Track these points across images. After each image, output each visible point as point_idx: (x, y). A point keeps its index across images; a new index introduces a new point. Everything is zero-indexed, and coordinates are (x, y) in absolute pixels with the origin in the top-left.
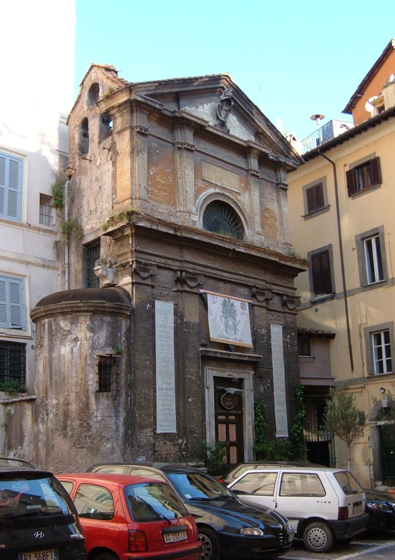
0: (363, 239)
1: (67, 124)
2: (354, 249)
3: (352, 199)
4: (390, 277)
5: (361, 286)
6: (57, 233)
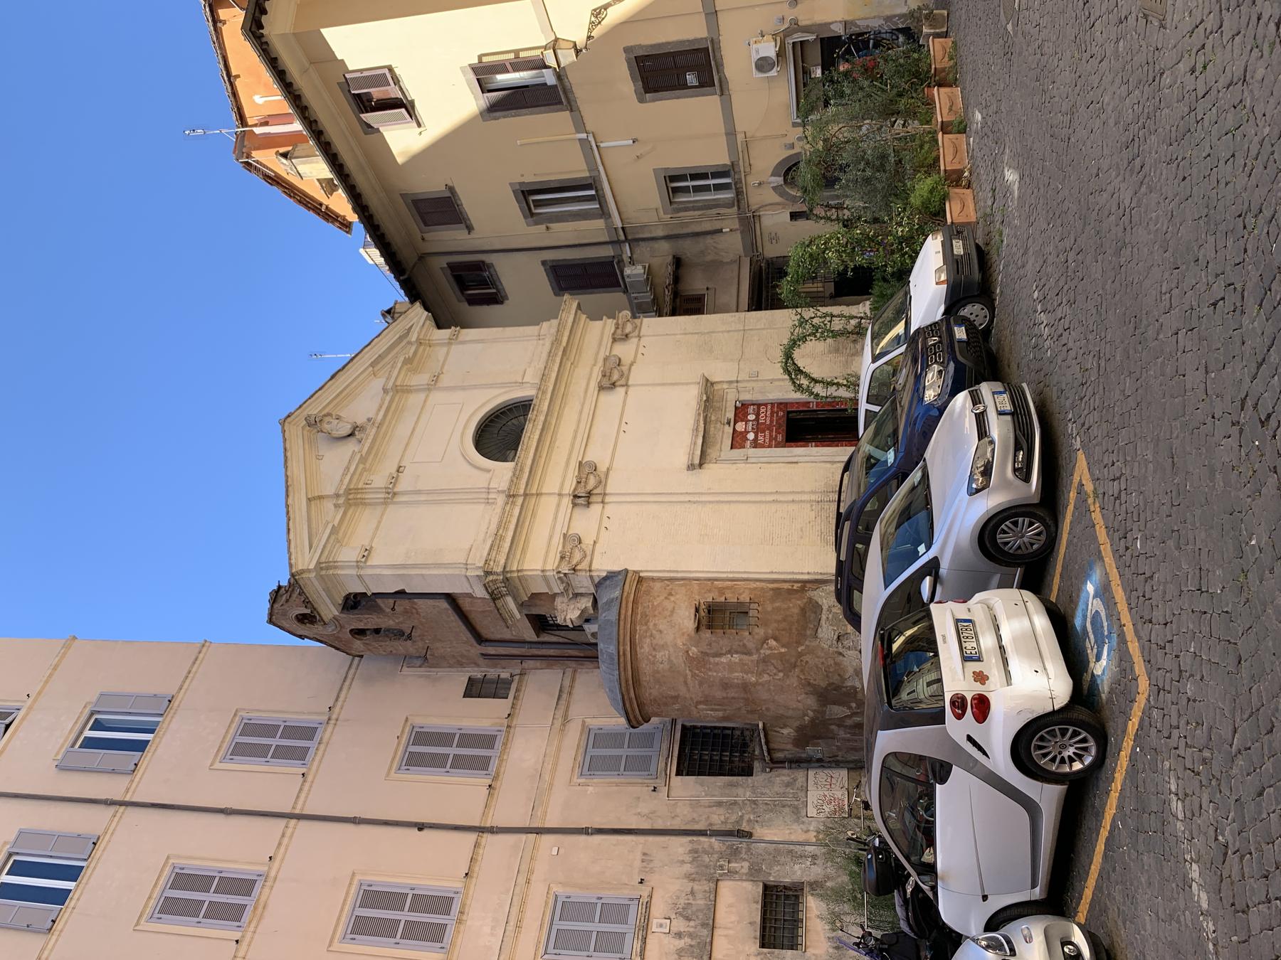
0: (532, 214)
1: (362, 656)
2: (547, 228)
3: (508, 299)
4: (587, 174)
5: (601, 218)
6: (703, 852)
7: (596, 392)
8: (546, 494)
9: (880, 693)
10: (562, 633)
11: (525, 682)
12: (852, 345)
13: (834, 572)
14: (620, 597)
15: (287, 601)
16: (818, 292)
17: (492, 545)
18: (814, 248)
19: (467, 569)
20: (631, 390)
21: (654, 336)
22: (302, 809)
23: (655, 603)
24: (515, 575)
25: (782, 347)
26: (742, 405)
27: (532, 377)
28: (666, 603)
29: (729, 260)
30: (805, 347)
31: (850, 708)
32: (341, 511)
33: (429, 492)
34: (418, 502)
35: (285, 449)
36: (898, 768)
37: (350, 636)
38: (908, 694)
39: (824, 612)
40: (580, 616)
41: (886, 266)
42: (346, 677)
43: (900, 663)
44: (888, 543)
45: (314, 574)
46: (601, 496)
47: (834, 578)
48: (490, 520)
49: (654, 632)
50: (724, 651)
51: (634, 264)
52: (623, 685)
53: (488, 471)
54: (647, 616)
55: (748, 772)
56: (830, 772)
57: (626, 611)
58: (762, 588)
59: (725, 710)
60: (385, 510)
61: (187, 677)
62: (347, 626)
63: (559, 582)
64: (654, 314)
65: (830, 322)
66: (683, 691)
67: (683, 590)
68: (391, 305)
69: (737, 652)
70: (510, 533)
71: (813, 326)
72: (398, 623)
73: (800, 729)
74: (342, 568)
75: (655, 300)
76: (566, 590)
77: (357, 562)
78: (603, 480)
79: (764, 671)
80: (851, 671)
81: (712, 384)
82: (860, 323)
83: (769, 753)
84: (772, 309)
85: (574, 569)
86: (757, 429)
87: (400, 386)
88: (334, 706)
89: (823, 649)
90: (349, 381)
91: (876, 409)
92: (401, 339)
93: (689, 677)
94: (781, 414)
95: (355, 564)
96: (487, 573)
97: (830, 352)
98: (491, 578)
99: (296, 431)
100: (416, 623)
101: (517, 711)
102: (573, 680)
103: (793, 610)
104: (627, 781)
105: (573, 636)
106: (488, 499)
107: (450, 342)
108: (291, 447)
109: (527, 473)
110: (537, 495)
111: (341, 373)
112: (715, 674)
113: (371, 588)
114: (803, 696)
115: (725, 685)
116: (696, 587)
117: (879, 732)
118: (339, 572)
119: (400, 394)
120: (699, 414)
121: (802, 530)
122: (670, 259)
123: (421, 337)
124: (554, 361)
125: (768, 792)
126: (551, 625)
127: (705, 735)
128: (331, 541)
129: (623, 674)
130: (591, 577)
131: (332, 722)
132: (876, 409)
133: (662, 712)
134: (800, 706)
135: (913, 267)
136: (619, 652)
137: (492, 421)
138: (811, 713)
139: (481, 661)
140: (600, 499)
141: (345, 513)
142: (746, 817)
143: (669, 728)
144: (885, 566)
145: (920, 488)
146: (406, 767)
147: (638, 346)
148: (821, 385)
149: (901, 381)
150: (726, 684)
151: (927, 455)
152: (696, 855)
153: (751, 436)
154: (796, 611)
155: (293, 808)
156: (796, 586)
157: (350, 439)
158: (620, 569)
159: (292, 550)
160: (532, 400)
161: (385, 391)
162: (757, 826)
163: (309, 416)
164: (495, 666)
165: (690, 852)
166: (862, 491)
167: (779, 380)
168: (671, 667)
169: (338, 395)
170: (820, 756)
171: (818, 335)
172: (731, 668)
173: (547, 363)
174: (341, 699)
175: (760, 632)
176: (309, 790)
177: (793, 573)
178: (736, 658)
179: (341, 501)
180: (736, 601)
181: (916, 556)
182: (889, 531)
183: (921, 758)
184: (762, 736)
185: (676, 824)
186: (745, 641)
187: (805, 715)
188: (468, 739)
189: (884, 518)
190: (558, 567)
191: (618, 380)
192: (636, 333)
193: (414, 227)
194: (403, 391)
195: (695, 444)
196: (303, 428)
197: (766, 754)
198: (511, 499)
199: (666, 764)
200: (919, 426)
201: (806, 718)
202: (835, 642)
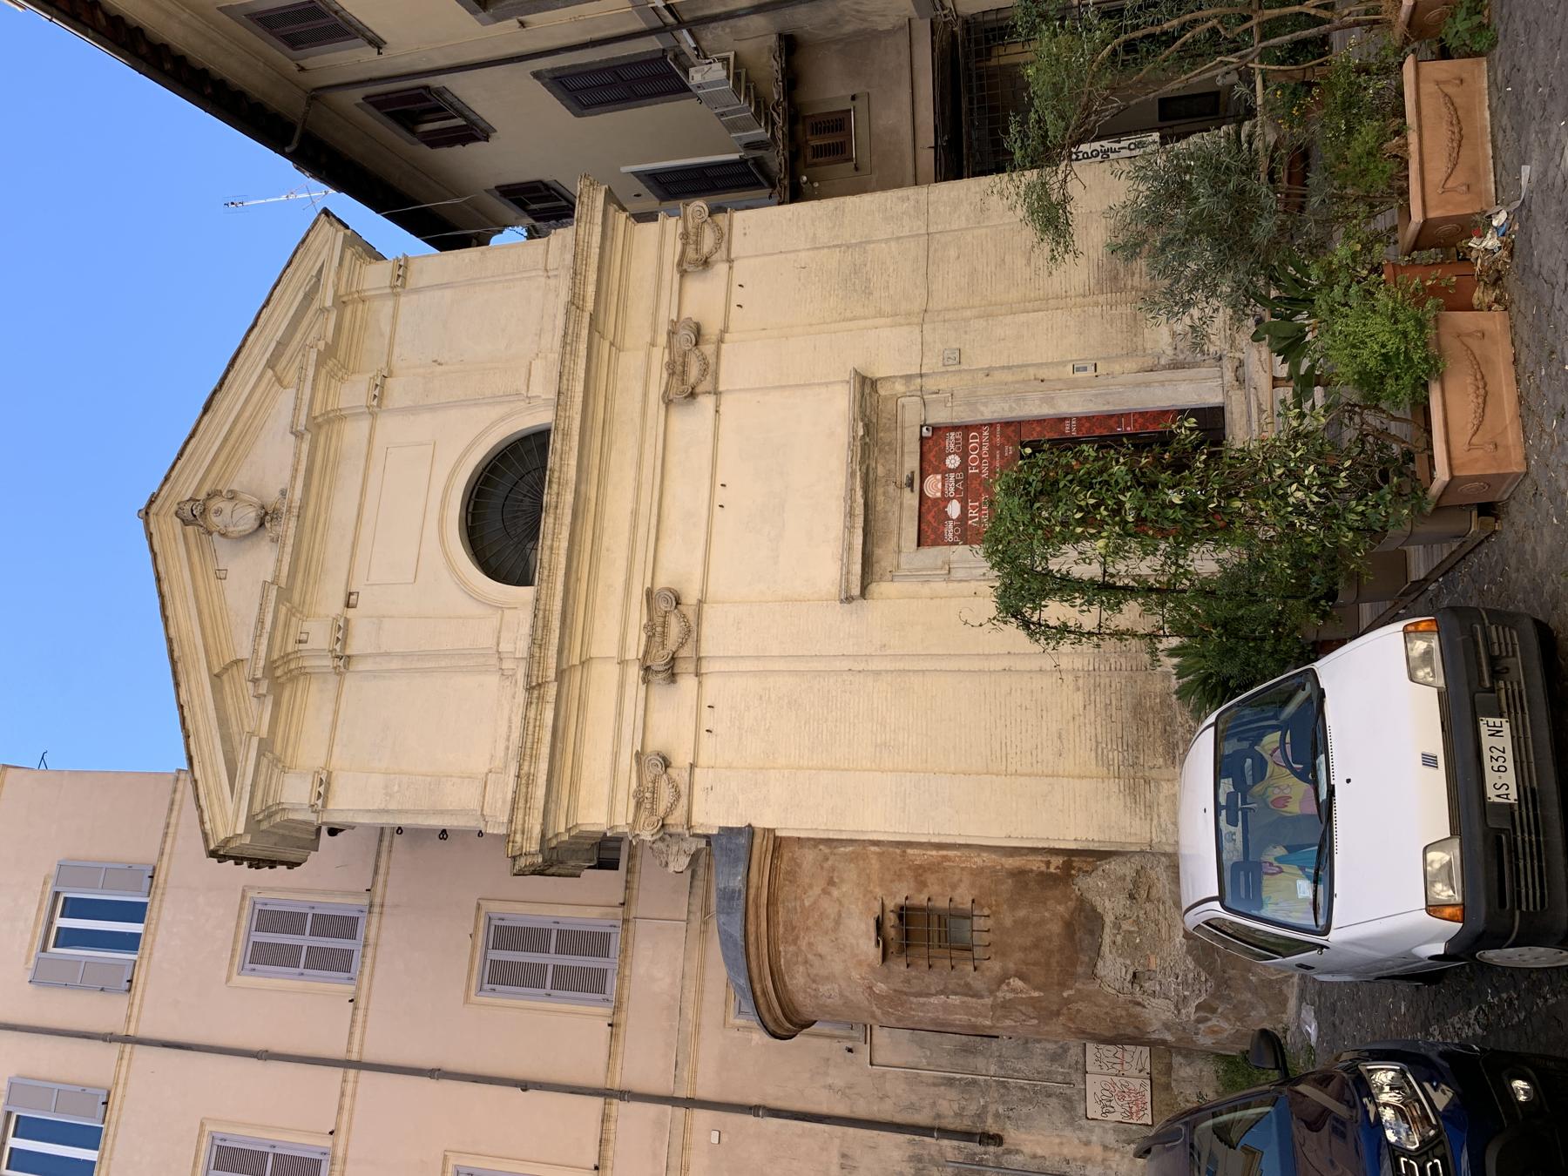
2: (522, 24)
6: (930, 1161)
20: (727, 402)
22: (360, 1053)
23: (807, 904)
27: (542, 387)
29: (889, 27)
32: (269, 701)
39: (1107, 930)
49: (810, 956)
50: (933, 991)
54: (794, 928)
57: (758, 926)
61: (166, 834)
69: (956, 994)
70: (543, 766)
81: (874, 383)
86: (966, 490)
87: (322, 415)
88: (373, 884)
89: (1106, 996)
90: (238, 407)
99: (168, 527)
101: (635, 892)
108: (167, 572)
109: (558, 631)
111: (219, 396)
116: (875, 864)
119: (325, 428)
120: (853, 474)
121: (1060, 737)
122: (773, 40)
124: (574, 353)
125: (1023, 1067)
128: (263, 769)
131: (376, 909)
141: (277, 704)
142: (992, 1108)
152: (920, 1166)
153: (954, 509)
154: (1056, 928)
155: (349, 1051)
159: (203, 802)
162: (1008, 1125)
165: (911, 1159)
169: (226, 439)
173: (562, 362)
174: (382, 871)
175: (995, 966)
176: (365, 1022)
185: (885, 1111)
188: (574, 941)
191: (699, 381)
192: (722, 253)
193: (278, 54)
194: (329, 421)
195: (850, 548)
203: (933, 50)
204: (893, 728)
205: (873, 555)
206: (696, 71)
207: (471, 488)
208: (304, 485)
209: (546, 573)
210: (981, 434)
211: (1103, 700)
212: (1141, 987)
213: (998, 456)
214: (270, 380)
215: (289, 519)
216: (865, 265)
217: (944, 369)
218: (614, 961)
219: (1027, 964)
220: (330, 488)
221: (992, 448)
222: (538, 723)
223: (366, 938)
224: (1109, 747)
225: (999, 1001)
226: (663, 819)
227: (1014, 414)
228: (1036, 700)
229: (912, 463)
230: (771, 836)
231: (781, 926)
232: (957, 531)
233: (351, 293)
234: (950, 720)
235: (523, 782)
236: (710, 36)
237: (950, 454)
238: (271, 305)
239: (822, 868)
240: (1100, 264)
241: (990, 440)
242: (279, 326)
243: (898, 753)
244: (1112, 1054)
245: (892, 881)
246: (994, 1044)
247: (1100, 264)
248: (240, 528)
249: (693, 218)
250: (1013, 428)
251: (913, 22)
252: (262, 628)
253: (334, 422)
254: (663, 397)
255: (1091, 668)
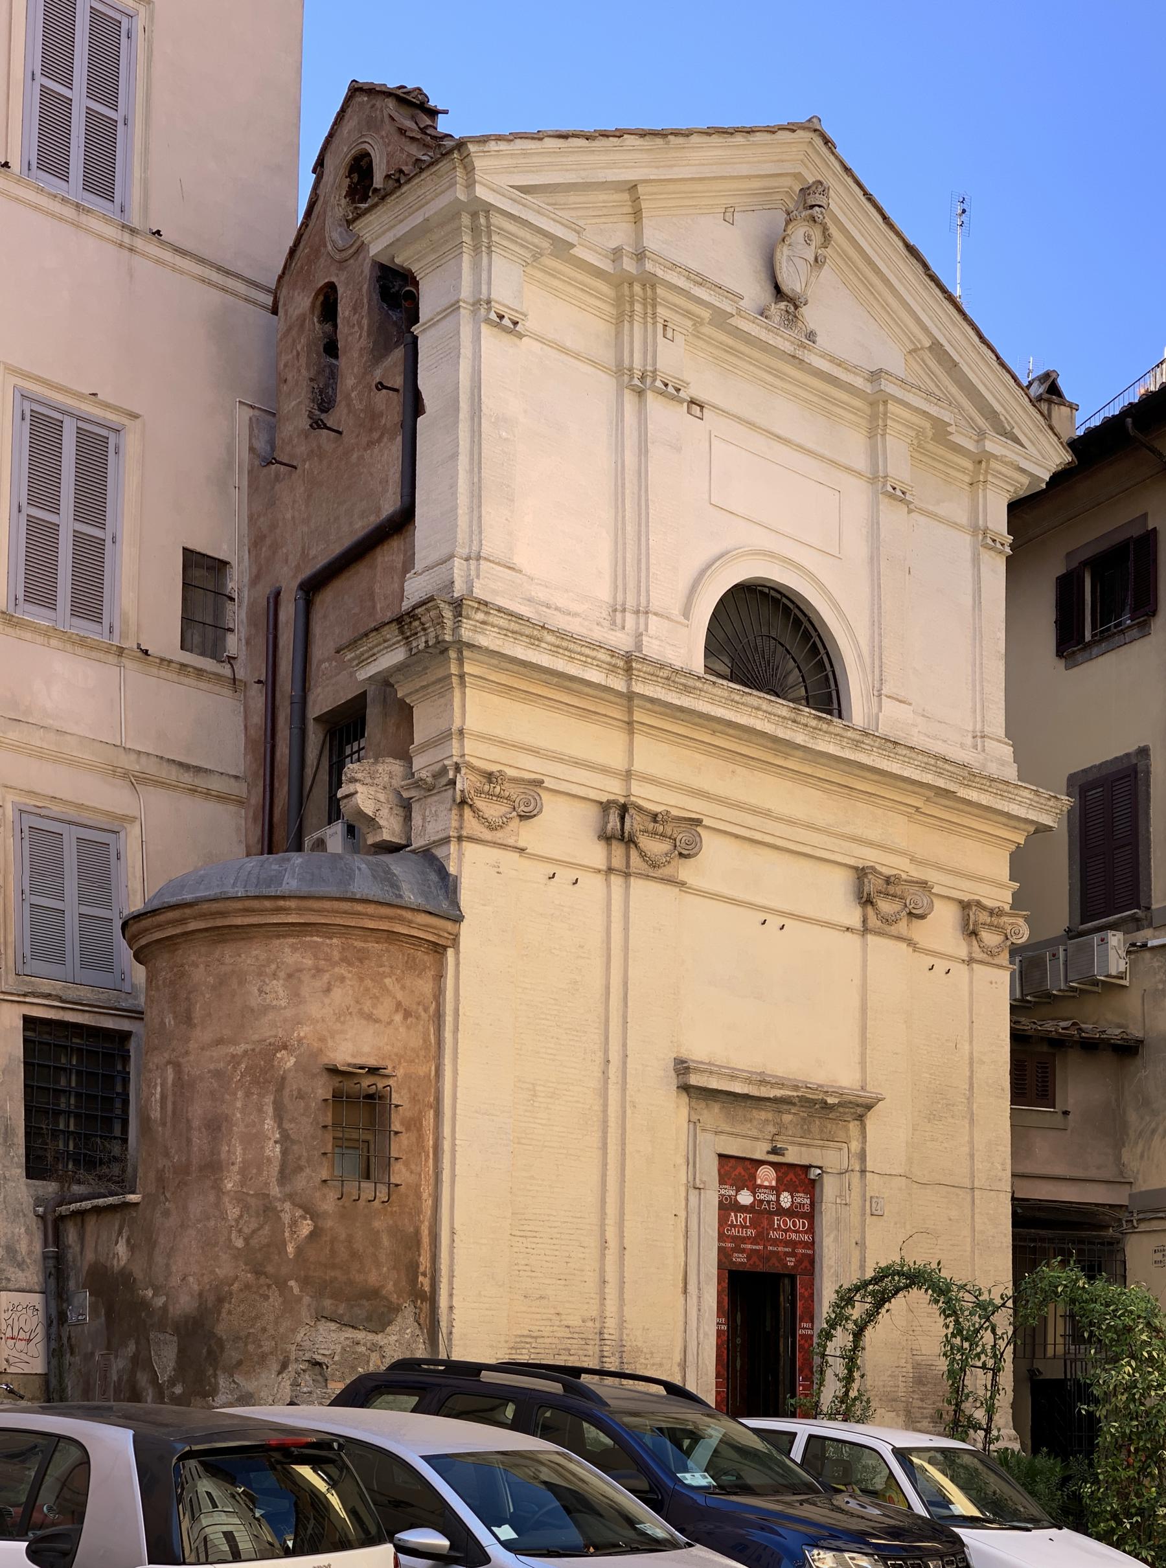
1: (275, 311)
7: (852, 862)
8: (631, 742)
9: (210, 1437)
10: (324, 776)
11: (217, 689)
12: (929, 1412)
13: (454, 1358)
14: (403, 903)
15: (402, 131)
16: (1045, 1345)
17: (519, 617)
18: (1144, 1337)
19: (467, 560)
20: (854, 940)
21: (971, 994)
23: (387, 981)
24: (454, 669)
25: (934, 1266)
26: (814, 1180)
28: (387, 1004)
29: (1125, 1159)
30: (929, 1315)
31: (172, 1382)
32: (606, 265)
33: (642, 474)
34: (619, 448)
35: (750, 131)
36: (59, 1467)
37: (321, 283)
38: (208, 1494)
39: (371, 1336)
40: (361, 814)
41: (1096, 1482)
42: (227, 273)
43: (270, 1480)
44: (517, 1465)
45: (463, 197)
46: (623, 868)
47: (443, 1356)
48: (576, 615)
51: (1129, 953)
52: (215, 906)
53: (686, 613)
54: (361, 960)
55: (35, 1168)
56: (38, 1338)
57: (371, 917)
58: (419, 1212)
59: (164, 1124)
60: (605, 369)
62: (343, 276)
63: (437, 767)
64: (1018, 996)
65: (984, 1367)
66: (203, 1035)
67: (416, 1042)
68: (1068, 396)
69: (284, 1153)
71: (977, 1331)
72: (348, 397)
73: (126, 1278)
74: (476, 266)
75: (1048, 999)
76: (418, 784)
77: (489, 302)
78: (658, 873)
79: (246, 1208)
80: (249, 1386)
81: (861, 1118)
82: (977, 1427)
83: (75, 1213)
84: (1015, 1248)
85: (463, 802)
86: (761, 1212)
89: (294, 1331)
91: (797, 1453)
92: (992, 416)
93: (231, 1049)
94: (791, 1262)
95: (484, 296)
96: (458, 606)
97: (917, 1366)
98: (448, 614)
100: (349, 439)
101: (155, 671)
102: (222, 798)
103: (374, 1272)
104: (11, 911)
105: (319, 796)
106: (624, 610)
107: (980, 532)
109: (678, 703)
110: (630, 723)
111: (920, 270)
112: (239, 1104)
113: (432, 332)
114: (196, 1287)
115: (216, 1126)
116: (422, 1070)
117: (131, 1432)
118: (466, 257)
120: (796, 1088)
121: (541, 1297)
122: (1136, 1032)
123: (994, 464)
124: (925, 768)
126: (341, 752)
127: (109, 1079)
128: (537, 240)
129: (239, 905)
130: (446, 841)
131: (127, 238)
132: (797, 1453)
133: (158, 989)
134: (175, 1281)
135: (1090, 1535)
136: (283, 898)
137: (797, 623)
138: (160, 1301)
139: (264, 590)
140: (618, 862)
141: (598, 273)
143: (124, 1005)
144: (471, 1460)
145: (631, 1534)
146: (28, 414)
147: (950, 958)
148: (850, 1345)
149: (853, 1505)
150: (219, 1128)
151: (700, 1552)
153: (745, 1198)
154: (373, 1279)
156: (424, 1282)
157: (770, 289)
158: (462, 904)
159: (520, 144)
160: (840, 717)
161: (875, 376)
163: (825, 192)
164: (252, 622)
166: (628, 1419)
167: (863, 1261)
168: (252, 1010)
170: (72, 1317)
171: (957, 1341)
172: (254, 1139)
174: (179, 261)
175: (328, 1203)
177: (452, 1277)
178: (273, 1151)
179: (629, 265)
180: (394, 1154)
181: (491, 1521)
182: (544, 1469)
183: (77, 1514)
184: (111, 1200)
186: (308, 1170)
187: (157, 1290)
189: (570, 1460)
190: (470, 767)
192: (978, 955)
194: (873, 418)
195: (733, 1077)
196: (797, 176)
197: (73, 1207)
198: (621, 664)
199: (48, 996)
200: (758, 1536)
201: (150, 1293)
202: (307, 1356)
203: (1097, 1205)
204: (550, 1106)
205: (716, 1101)
206: (1119, 940)
207: (793, 598)
208: (823, 372)
209: (737, 698)
210: (806, 1232)
211: (574, 1346)
212: (304, 1371)
213: (787, 1250)
214: (919, 341)
215: (793, 343)
216: (953, 1117)
217: (868, 1198)
218: (67, 625)
219: (332, 1242)
220: (805, 400)
221: (794, 1244)
222: (589, 660)
223: (89, 211)
224: (532, 1350)
225: (278, 1204)
226: (471, 805)
227: (825, 1269)
228: (574, 1275)
229: (793, 1156)
230: (449, 943)
231: (362, 944)
232: (726, 1199)
233: (986, 472)
234: (558, 1176)
235: (536, 633)
236: (1156, 964)
237: (792, 1198)
238: (998, 367)
239: (419, 1004)
240: (934, 1368)
241: (801, 1242)
242: (973, 371)
243: (526, 1111)
244: (22, 1325)
245: (409, 1089)
246: (19, 1171)
247: (934, 1368)
248: (784, 264)
249: (1012, 924)
250: (808, 1265)
251: (1128, 1186)
252: (696, 283)
253: (870, 422)
254: (872, 868)
255: (606, 1336)
